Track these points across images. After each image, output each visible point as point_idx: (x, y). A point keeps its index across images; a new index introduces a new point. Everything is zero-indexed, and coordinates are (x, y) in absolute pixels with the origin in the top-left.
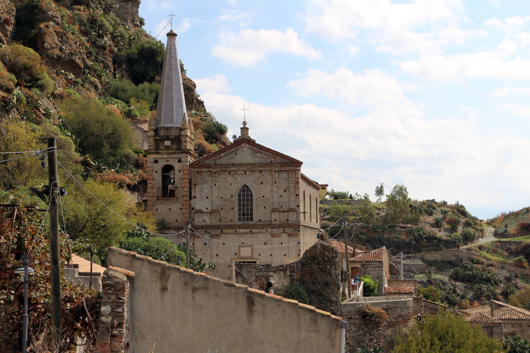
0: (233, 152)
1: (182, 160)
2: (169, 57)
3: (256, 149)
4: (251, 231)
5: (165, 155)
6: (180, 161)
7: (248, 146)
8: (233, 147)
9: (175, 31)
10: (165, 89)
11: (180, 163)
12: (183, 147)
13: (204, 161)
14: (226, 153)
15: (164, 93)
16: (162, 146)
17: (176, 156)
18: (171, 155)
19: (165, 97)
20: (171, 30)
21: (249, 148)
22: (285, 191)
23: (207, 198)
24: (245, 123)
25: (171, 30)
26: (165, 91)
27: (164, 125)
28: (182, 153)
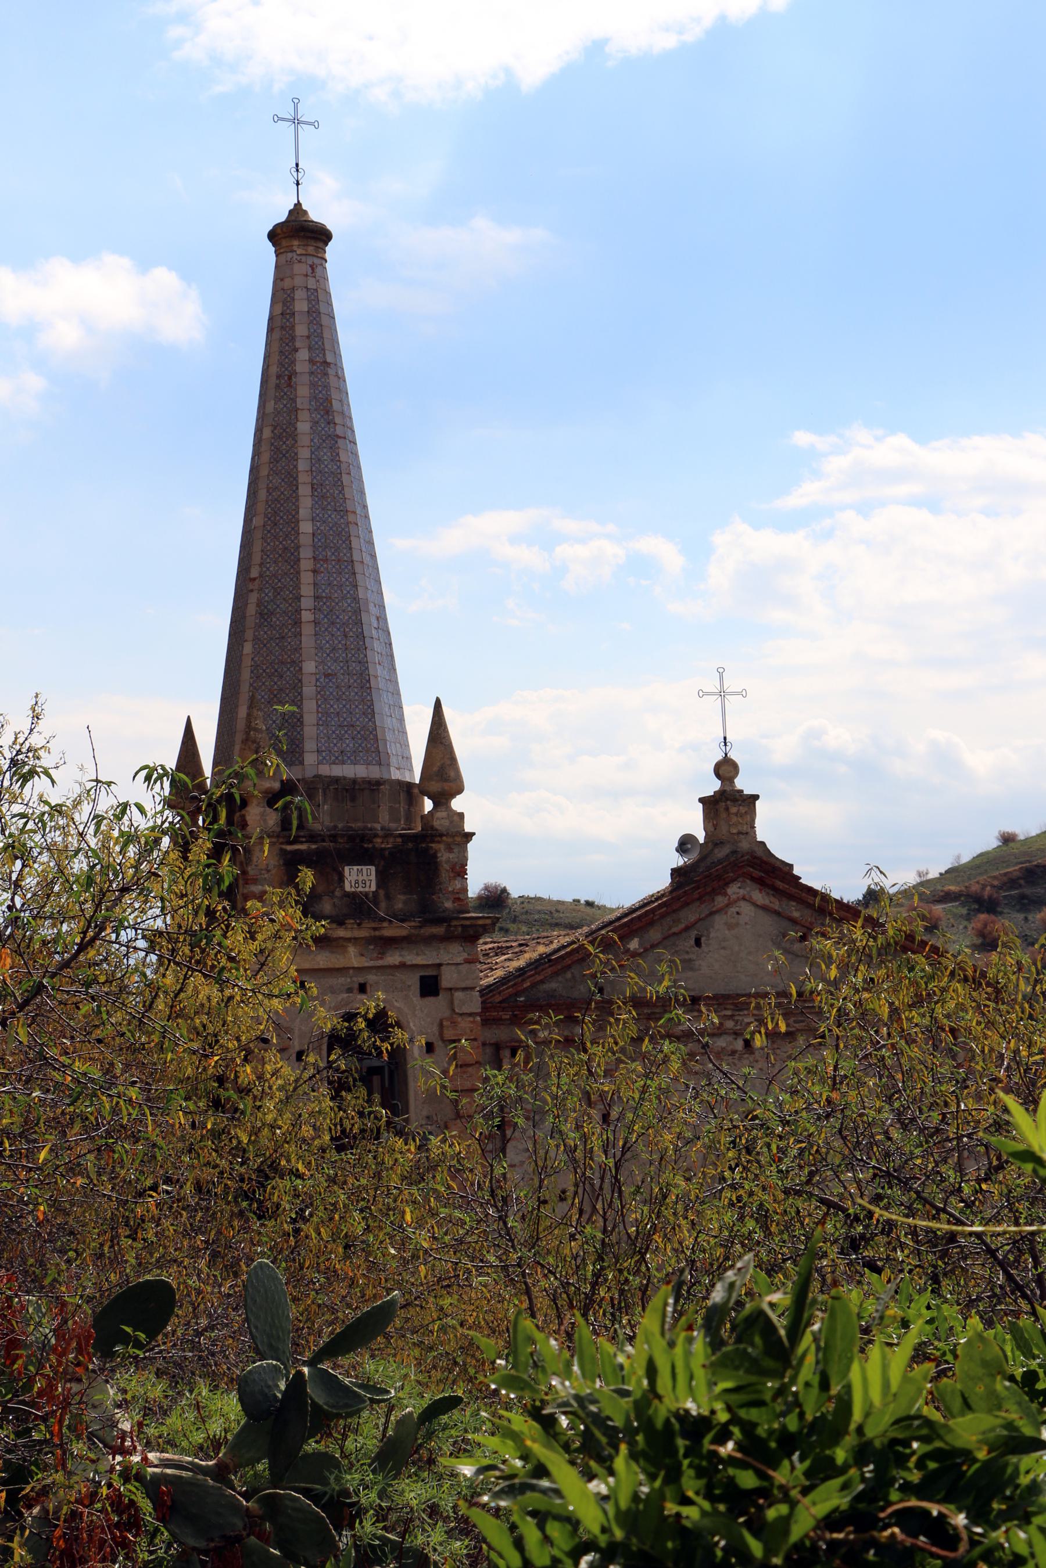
0: (687, 929)
1: (448, 978)
2: (311, 361)
3: (796, 914)
5: (352, 950)
6: (430, 986)
8: (687, 904)
9: (316, 215)
10: (306, 553)
11: (430, 1000)
12: (448, 904)
13: (542, 982)
14: (655, 934)
15: (307, 578)
16: (331, 894)
17: (412, 958)
18: (382, 955)
19: (317, 598)
20: (297, 210)
21: (764, 908)
24: (726, 769)
25: (297, 210)
26: (306, 565)
27: (325, 770)
28: (447, 938)
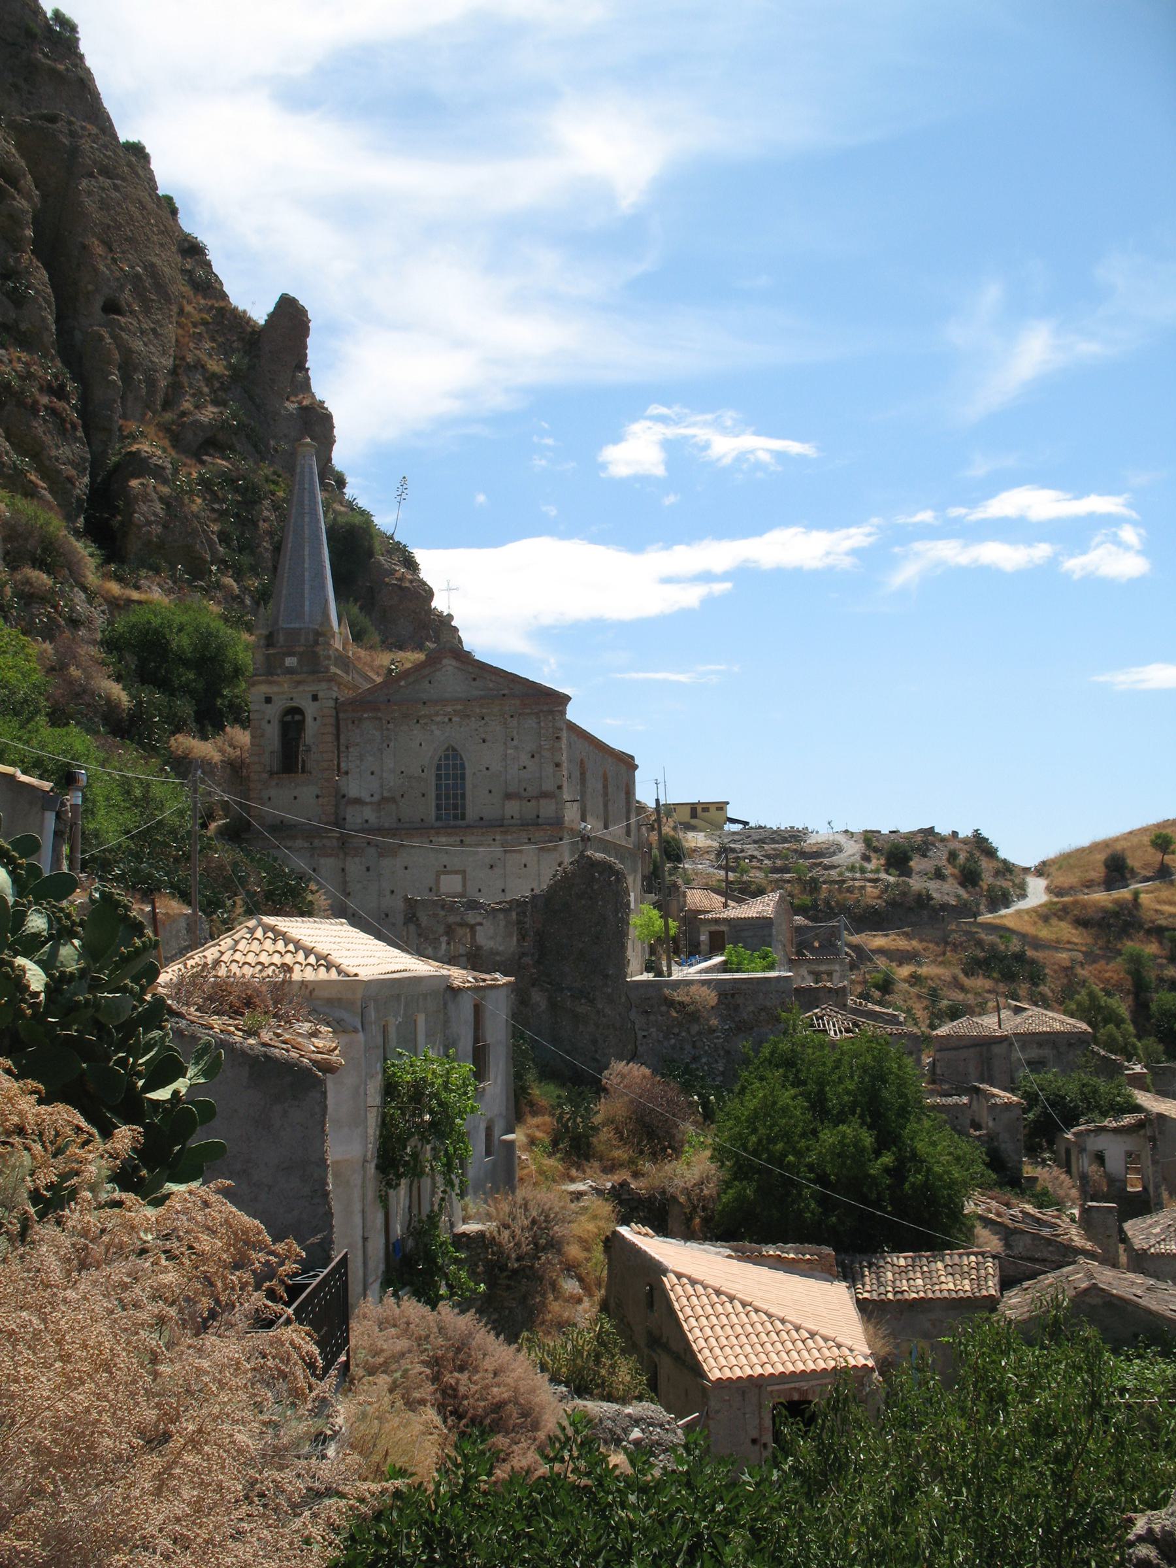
4: (462, 841)
7: (454, 663)
22: (533, 756)
23: (372, 773)
